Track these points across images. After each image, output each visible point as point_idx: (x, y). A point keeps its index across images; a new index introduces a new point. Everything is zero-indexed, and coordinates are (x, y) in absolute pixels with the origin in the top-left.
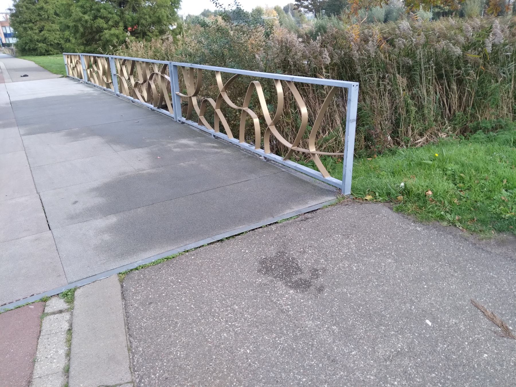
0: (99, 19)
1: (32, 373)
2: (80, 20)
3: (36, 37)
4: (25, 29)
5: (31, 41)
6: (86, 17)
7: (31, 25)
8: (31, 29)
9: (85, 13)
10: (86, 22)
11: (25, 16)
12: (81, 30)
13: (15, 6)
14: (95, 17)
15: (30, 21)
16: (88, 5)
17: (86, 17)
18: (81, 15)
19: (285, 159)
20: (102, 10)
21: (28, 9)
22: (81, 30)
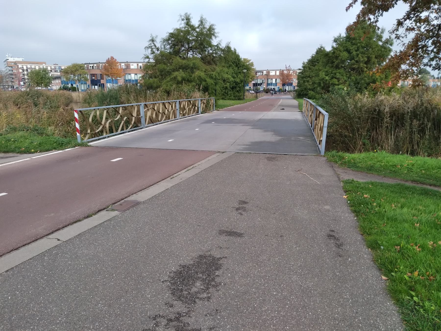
0: (334, 79)
1: (13, 151)
2: (323, 79)
3: (309, 87)
4: (304, 82)
5: (305, 89)
6: (327, 78)
7: (309, 79)
8: (308, 81)
9: (327, 75)
10: (326, 80)
11: (307, 74)
12: (322, 85)
13: (303, 67)
14: (333, 78)
15: (309, 77)
16: (330, 70)
17: (327, 78)
18: (324, 76)
19: (338, 152)
20: (337, 74)
21: (310, 69)
22: (322, 85)
